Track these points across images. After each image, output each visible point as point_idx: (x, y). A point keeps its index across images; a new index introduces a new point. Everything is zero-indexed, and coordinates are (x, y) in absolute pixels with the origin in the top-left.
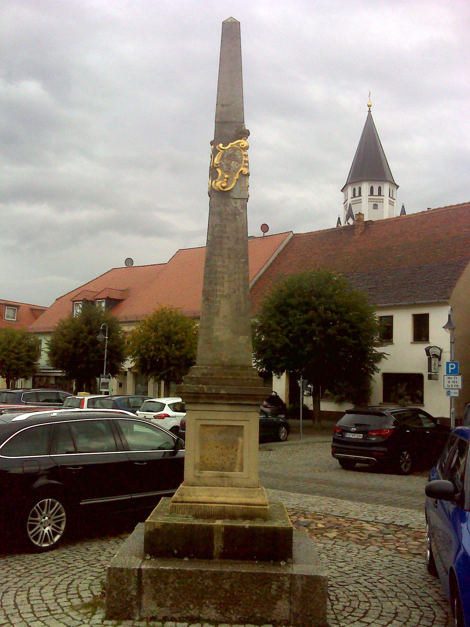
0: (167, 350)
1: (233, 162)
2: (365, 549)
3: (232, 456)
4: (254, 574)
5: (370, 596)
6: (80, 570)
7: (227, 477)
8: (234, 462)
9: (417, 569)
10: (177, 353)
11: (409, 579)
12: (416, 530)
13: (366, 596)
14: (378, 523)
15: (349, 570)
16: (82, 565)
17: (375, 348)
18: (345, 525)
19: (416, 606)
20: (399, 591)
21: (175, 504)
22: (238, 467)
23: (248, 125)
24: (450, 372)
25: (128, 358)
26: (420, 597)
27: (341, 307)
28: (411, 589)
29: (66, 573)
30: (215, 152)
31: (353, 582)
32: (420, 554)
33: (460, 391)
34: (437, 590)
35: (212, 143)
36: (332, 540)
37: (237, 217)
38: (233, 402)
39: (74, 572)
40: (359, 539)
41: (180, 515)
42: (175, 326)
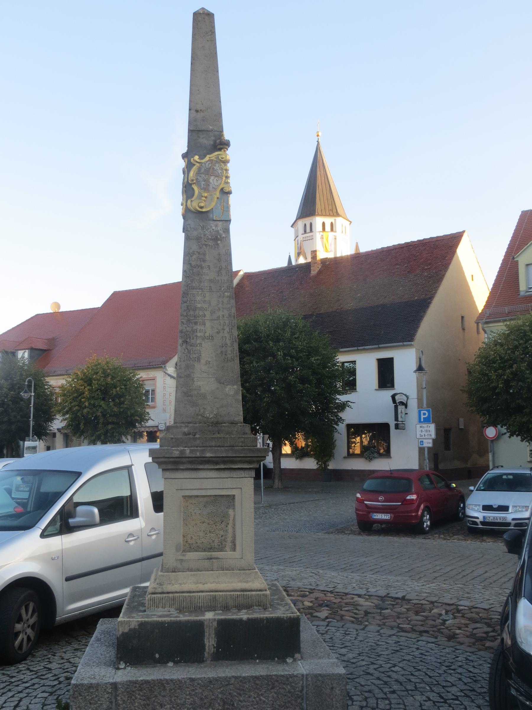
0: (103, 406)
1: (212, 178)
2: (363, 629)
3: (222, 533)
4: (256, 678)
5: (386, 690)
6: (27, 685)
7: (217, 558)
8: (225, 540)
9: (429, 650)
10: (115, 409)
11: (423, 664)
12: (414, 602)
13: (382, 690)
14: (372, 596)
15: (354, 658)
16: (29, 678)
17: (338, 396)
18: (335, 601)
19: (442, 700)
20: (418, 681)
21: (153, 596)
22: (229, 545)
23: (227, 135)
24: (422, 420)
25: (58, 416)
26: (443, 687)
27: (301, 351)
28: (430, 677)
29: (10, 690)
30: (189, 166)
31: (362, 673)
32: (426, 632)
33: (434, 441)
34: (460, 676)
35: (184, 156)
36: (324, 620)
37: (219, 242)
38: (222, 466)
39: (20, 689)
40: (354, 618)
41: (161, 609)
42: (113, 378)
